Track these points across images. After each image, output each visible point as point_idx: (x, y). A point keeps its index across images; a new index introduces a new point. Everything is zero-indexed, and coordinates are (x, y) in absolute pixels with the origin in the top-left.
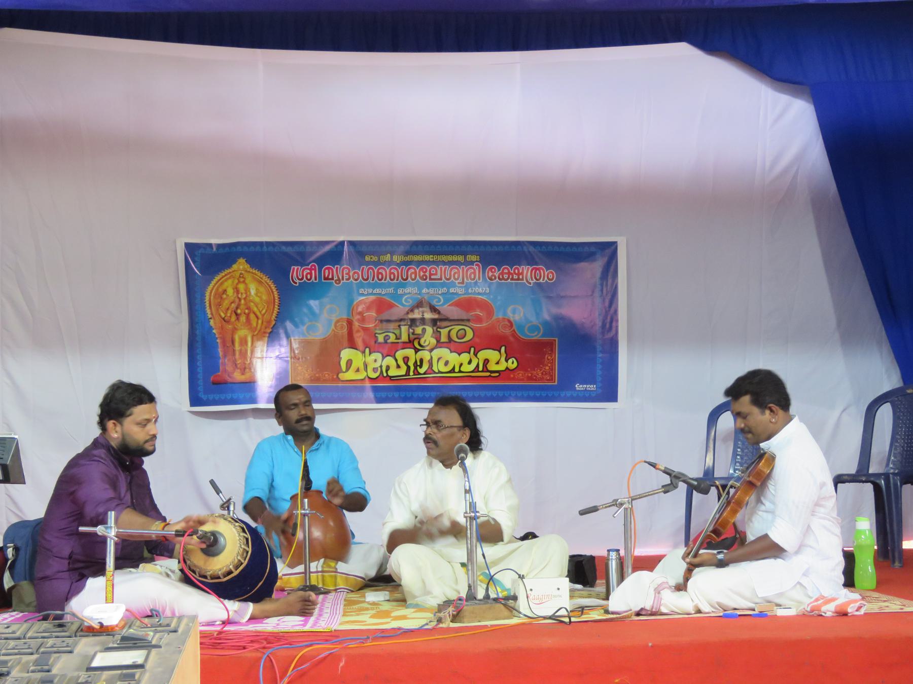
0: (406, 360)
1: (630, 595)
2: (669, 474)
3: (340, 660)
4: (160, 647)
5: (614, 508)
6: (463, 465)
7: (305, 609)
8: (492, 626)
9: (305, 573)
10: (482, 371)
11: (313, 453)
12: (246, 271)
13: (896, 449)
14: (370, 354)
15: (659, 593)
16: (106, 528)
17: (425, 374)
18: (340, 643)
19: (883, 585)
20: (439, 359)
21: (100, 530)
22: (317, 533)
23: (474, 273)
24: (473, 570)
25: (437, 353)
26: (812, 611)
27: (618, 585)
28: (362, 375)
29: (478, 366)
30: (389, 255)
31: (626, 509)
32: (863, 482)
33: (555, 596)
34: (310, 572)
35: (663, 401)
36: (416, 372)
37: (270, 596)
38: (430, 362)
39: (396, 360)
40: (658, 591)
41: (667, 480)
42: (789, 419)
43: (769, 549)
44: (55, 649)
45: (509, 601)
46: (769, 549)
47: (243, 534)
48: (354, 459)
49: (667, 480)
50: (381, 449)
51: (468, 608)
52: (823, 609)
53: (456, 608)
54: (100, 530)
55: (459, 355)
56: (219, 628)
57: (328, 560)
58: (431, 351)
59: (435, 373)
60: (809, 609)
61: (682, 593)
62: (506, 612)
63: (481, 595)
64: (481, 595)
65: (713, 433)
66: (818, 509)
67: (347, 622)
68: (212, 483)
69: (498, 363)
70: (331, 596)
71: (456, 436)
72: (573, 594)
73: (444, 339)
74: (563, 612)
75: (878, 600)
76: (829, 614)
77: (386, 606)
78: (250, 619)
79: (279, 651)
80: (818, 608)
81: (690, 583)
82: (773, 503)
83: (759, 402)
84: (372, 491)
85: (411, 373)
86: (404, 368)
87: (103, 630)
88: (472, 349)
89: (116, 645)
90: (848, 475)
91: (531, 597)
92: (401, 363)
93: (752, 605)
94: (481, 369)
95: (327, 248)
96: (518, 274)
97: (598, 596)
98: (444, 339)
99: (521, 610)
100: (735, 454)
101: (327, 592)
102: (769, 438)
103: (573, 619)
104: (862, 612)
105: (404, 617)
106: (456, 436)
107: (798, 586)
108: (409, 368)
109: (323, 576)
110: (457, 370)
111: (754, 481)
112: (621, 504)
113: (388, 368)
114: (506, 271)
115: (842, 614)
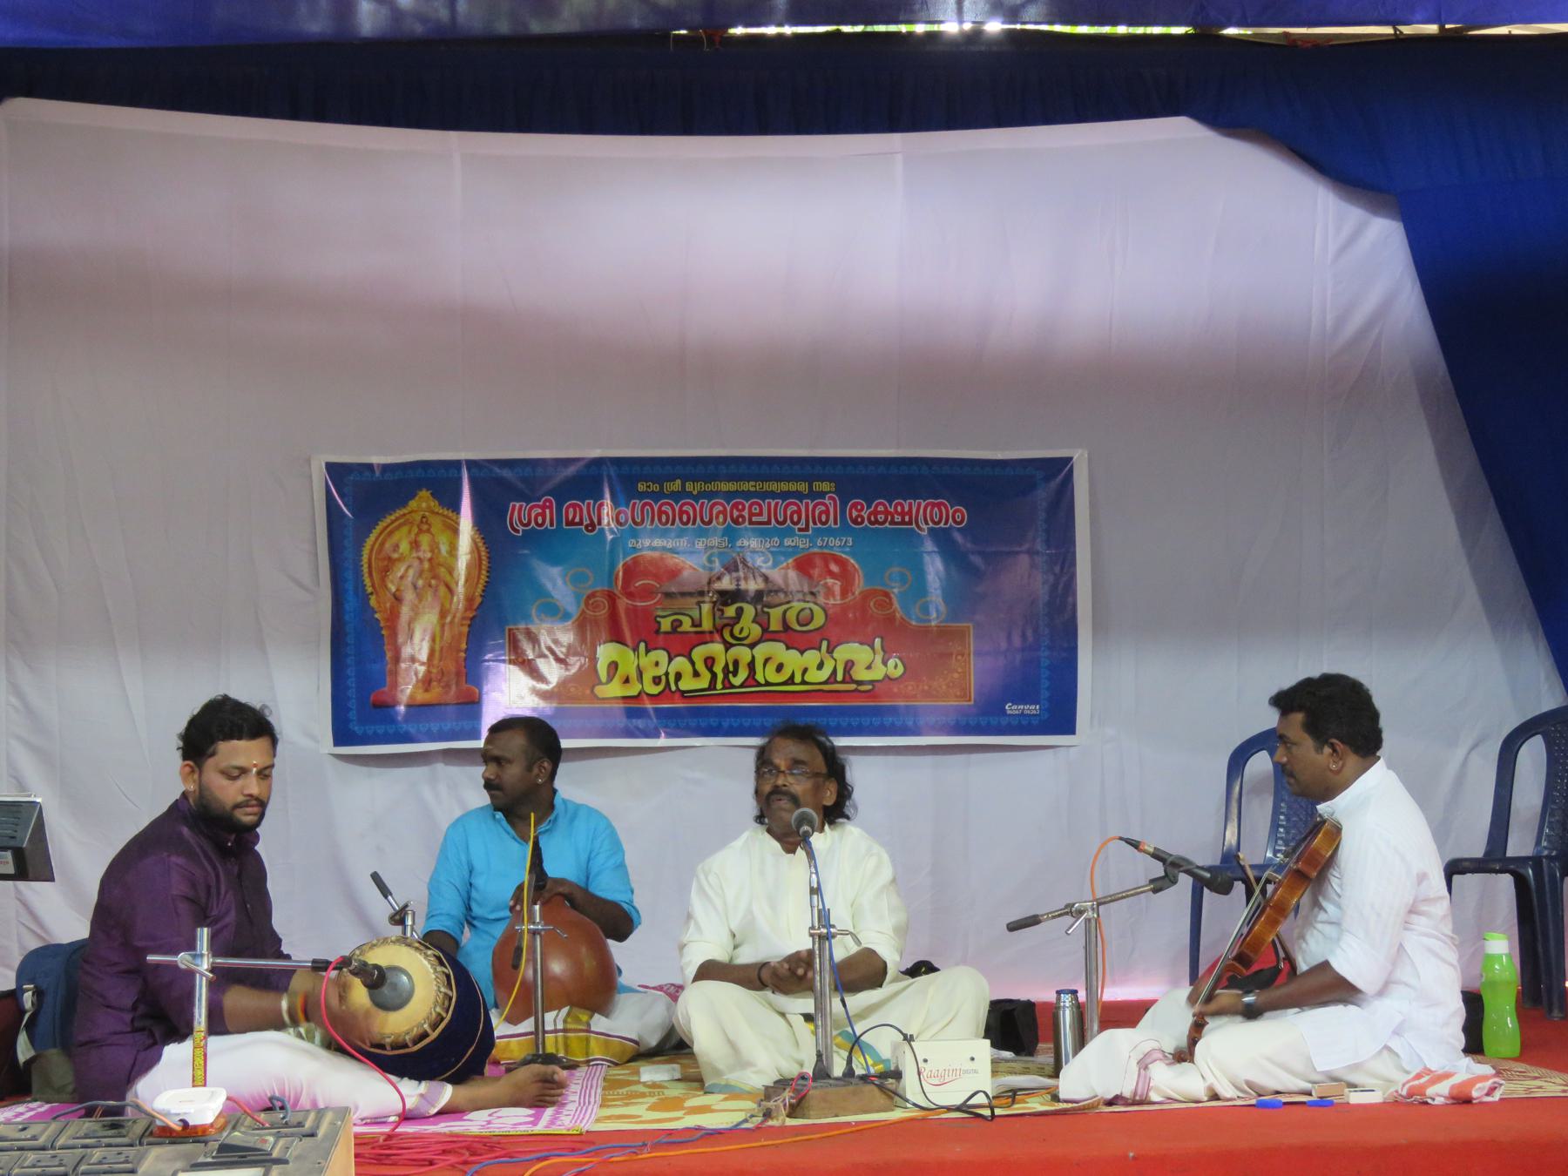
1: (1097, 1070)
5: (1068, 919)
7: (545, 1095)
8: (857, 1123)
9: (536, 1033)
10: (843, 682)
13: (1552, 815)
14: (647, 651)
15: (1146, 1068)
16: (194, 957)
17: (742, 686)
18: (597, 1153)
19: (1534, 1050)
20: (767, 661)
21: (182, 959)
22: (557, 967)
23: (827, 512)
24: (824, 1025)
25: (762, 651)
26: (1410, 1095)
27: (1075, 1053)
28: (633, 690)
29: (834, 672)
30: (678, 482)
31: (1088, 921)
33: (966, 1072)
34: (544, 1032)
35: (1159, 733)
36: (727, 684)
38: (751, 666)
39: (693, 663)
40: (1144, 1065)
41: (1158, 870)
43: (1332, 988)
44: (105, 1167)
45: (887, 1081)
46: (1332, 988)
48: (617, 847)
49: (1158, 870)
51: (815, 1092)
52: (1430, 1091)
53: (794, 1092)
54: (182, 959)
55: (802, 653)
57: (576, 1011)
58: (752, 646)
59: (759, 685)
60: (1404, 1093)
62: (881, 1099)
63: (838, 1069)
64: (838, 1069)
66: (1414, 918)
67: (609, 1118)
68: (376, 877)
69: (869, 667)
70: (581, 1072)
71: (803, 794)
72: (996, 1068)
73: (775, 625)
74: (980, 1099)
75: (1523, 1076)
76: (1439, 1101)
77: (677, 1091)
80: (1420, 1090)
82: (1339, 906)
83: (1317, 730)
84: (642, 902)
85: (719, 686)
86: (706, 676)
87: (188, 1133)
88: (825, 644)
91: (924, 1074)
92: (700, 667)
93: (1308, 1086)
94: (840, 678)
95: (571, 470)
96: (903, 514)
97: (1041, 1072)
98: (775, 625)
99: (908, 1096)
100: (1275, 825)
101: (572, 1066)
102: (1329, 793)
103: (998, 1112)
104: (1497, 1096)
106: (803, 794)
107: (1385, 1053)
108: (714, 676)
109: (566, 1038)
110: (798, 679)
112: (1080, 912)
113: (678, 676)
114: (881, 508)
115: (1462, 1099)
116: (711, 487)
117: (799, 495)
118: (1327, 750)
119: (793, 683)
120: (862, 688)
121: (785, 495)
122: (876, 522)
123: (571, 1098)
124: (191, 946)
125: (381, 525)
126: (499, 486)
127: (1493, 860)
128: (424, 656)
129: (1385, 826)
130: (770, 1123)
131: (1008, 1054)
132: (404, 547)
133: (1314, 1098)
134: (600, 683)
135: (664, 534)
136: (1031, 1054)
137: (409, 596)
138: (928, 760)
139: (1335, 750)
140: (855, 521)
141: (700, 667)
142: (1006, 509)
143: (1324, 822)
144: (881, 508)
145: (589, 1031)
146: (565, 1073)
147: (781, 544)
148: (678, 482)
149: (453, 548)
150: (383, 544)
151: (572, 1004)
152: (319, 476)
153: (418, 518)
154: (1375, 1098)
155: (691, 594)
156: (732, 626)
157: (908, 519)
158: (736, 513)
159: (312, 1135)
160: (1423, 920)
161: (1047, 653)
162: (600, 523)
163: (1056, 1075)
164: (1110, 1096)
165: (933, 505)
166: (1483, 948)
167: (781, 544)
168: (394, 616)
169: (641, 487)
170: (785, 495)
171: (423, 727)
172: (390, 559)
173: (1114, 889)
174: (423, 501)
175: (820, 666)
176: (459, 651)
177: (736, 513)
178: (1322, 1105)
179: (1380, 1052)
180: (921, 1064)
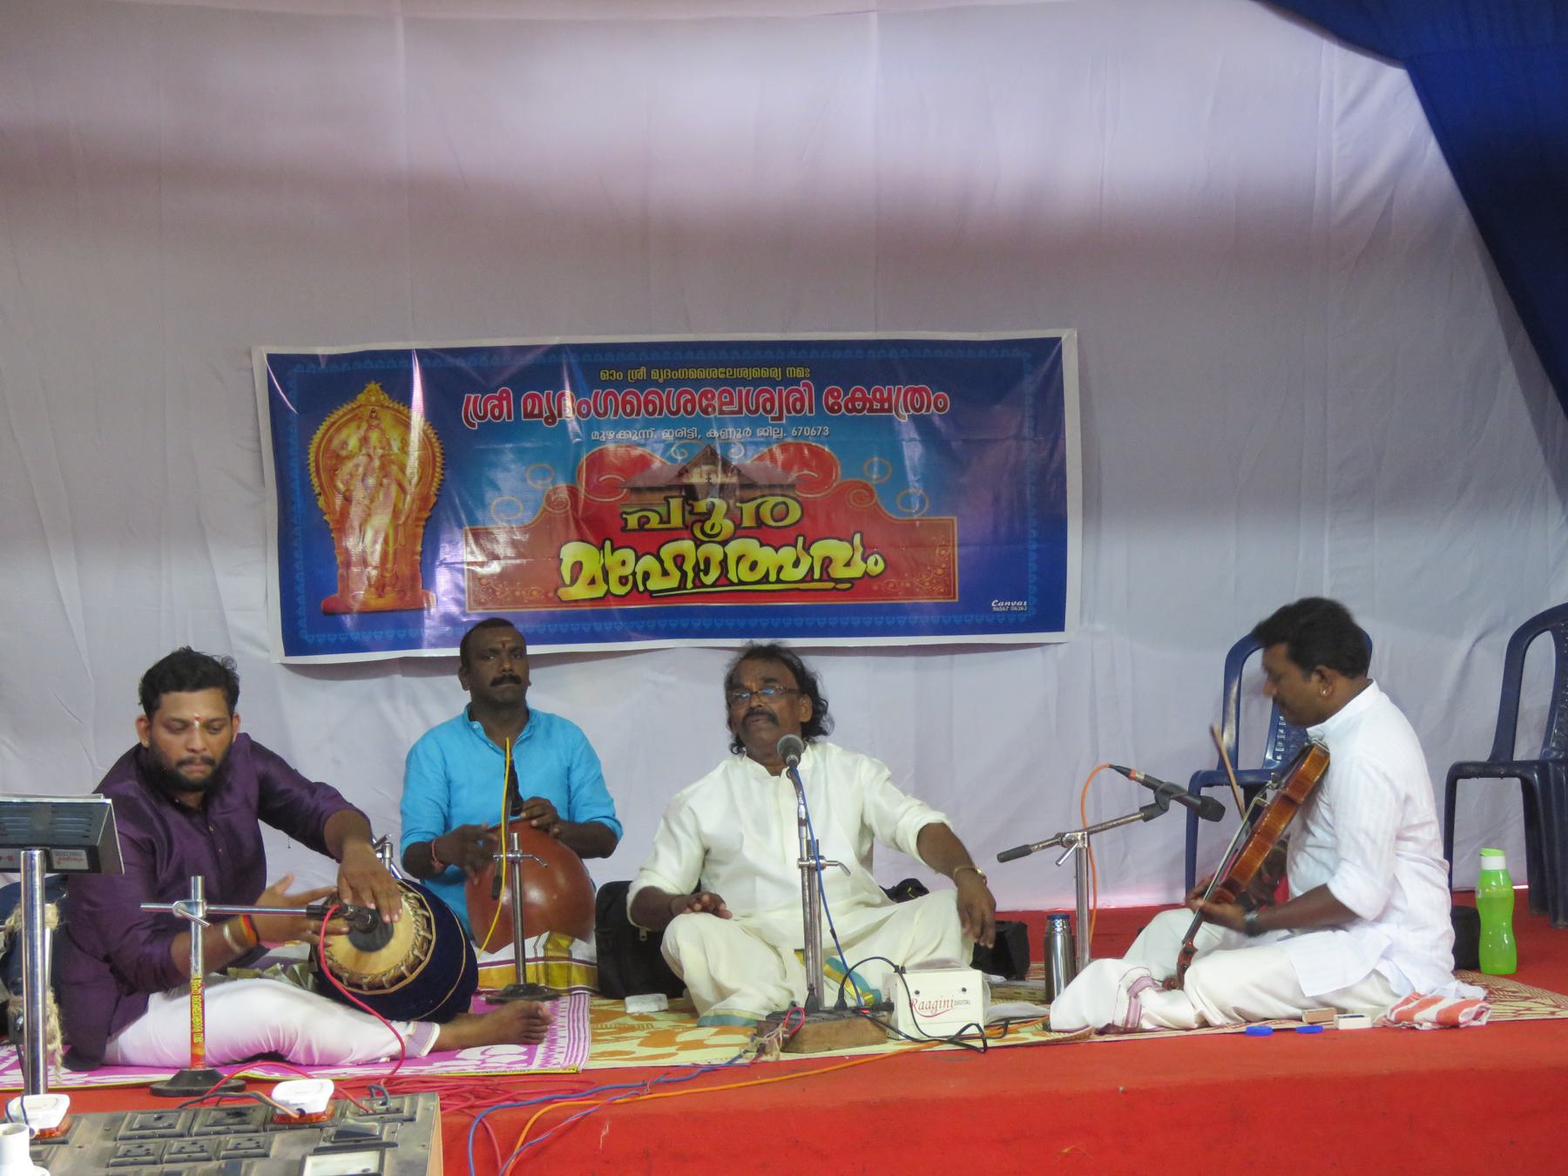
0: (679, 560)
1: (1091, 998)
2: (1153, 787)
3: (602, 1126)
4: (394, 1145)
5: (1059, 849)
6: (793, 775)
7: (530, 1031)
8: (852, 1057)
9: (516, 961)
10: (820, 580)
11: (523, 746)
12: (382, 406)
13: (1561, 715)
14: (613, 550)
15: (1136, 996)
16: (189, 905)
17: (713, 585)
18: (598, 1095)
19: (1534, 966)
20: (740, 558)
21: (178, 908)
22: (535, 895)
23: (802, 400)
24: (815, 957)
25: (734, 548)
26: (1398, 1021)
27: (1068, 982)
28: (599, 591)
29: (811, 569)
30: (643, 369)
31: (1079, 851)
32: (1502, 777)
33: (958, 1003)
34: (525, 960)
36: (698, 582)
37: (466, 1010)
38: (724, 564)
39: (661, 562)
40: (1134, 993)
41: (1149, 797)
42: (1367, 684)
43: (1327, 912)
45: (878, 1012)
46: (1327, 912)
47: (420, 912)
48: (593, 759)
49: (1149, 797)
50: (639, 731)
51: (809, 1027)
52: (1418, 1017)
53: (787, 1024)
54: (178, 908)
55: (777, 550)
56: (387, 1071)
57: (556, 936)
58: (724, 543)
59: (732, 584)
60: (1393, 1018)
61: (1175, 992)
63: (830, 1000)
64: (830, 1000)
65: (1235, 689)
66: (1403, 844)
67: (602, 1054)
69: (848, 564)
70: (564, 1003)
71: (776, 721)
72: (995, 993)
73: (748, 521)
74: (973, 1030)
75: (1515, 996)
76: (1427, 1026)
77: (665, 1023)
78: (432, 1051)
79: (500, 1114)
80: (1408, 1016)
81: (1188, 975)
83: (1303, 659)
85: (689, 584)
86: (676, 575)
87: (304, 1120)
88: (800, 540)
89: (328, 1144)
90: (1476, 764)
92: (670, 565)
93: (1298, 1012)
94: (817, 575)
95: (529, 358)
96: (882, 401)
97: (1032, 998)
98: (748, 521)
99: (901, 1028)
100: (1275, 726)
101: (555, 996)
102: (1321, 718)
103: (990, 1043)
104: (1484, 1020)
105: (698, 1045)
106: (776, 721)
108: (684, 575)
109: (547, 967)
110: (773, 577)
111: (1294, 796)
112: (1071, 842)
113: (646, 576)
115: (1448, 1024)
116: (679, 374)
117: (772, 382)
118: (1315, 677)
119: (768, 582)
120: (840, 586)
121: (756, 382)
122: (855, 409)
123: (561, 1033)
124: (185, 894)
125: (329, 420)
126: (454, 375)
127: (1499, 764)
128: (375, 559)
129: (1375, 750)
130: (764, 1058)
131: (997, 979)
132: (353, 443)
133: (1304, 1024)
134: (564, 585)
135: (628, 426)
136: (1023, 979)
137: (359, 494)
138: (910, 661)
139: (1323, 677)
140: (831, 409)
141: (670, 565)
142: (1002, 384)
143: (1311, 746)
144: (859, 395)
145: (570, 959)
146: (547, 1005)
147: (754, 434)
148: (643, 369)
149: (405, 443)
150: (330, 441)
151: (552, 930)
152: (260, 366)
153: (367, 413)
154: (1364, 1023)
155: (660, 489)
156: (703, 522)
157: (887, 406)
158: (704, 403)
159: (412, 1120)
160: (1410, 845)
161: (1034, 546)
162: (560, 415)
163: (1049, 998)
164: (1101, 1025)
165: (915, 391)
166: (1479, 863)
167: (754, 434)
168: (344, 515)
169: (604, 375)
170: (756, 382)
171: (378, 635)
172: (338, 456)
173: (1106, 818)
174: (372, 394)
175: (796, 564)
176: (414, 553)
177: (704, 403)
178: (1311, 1032)
179: (1369, 976)
180: (913, 996)
